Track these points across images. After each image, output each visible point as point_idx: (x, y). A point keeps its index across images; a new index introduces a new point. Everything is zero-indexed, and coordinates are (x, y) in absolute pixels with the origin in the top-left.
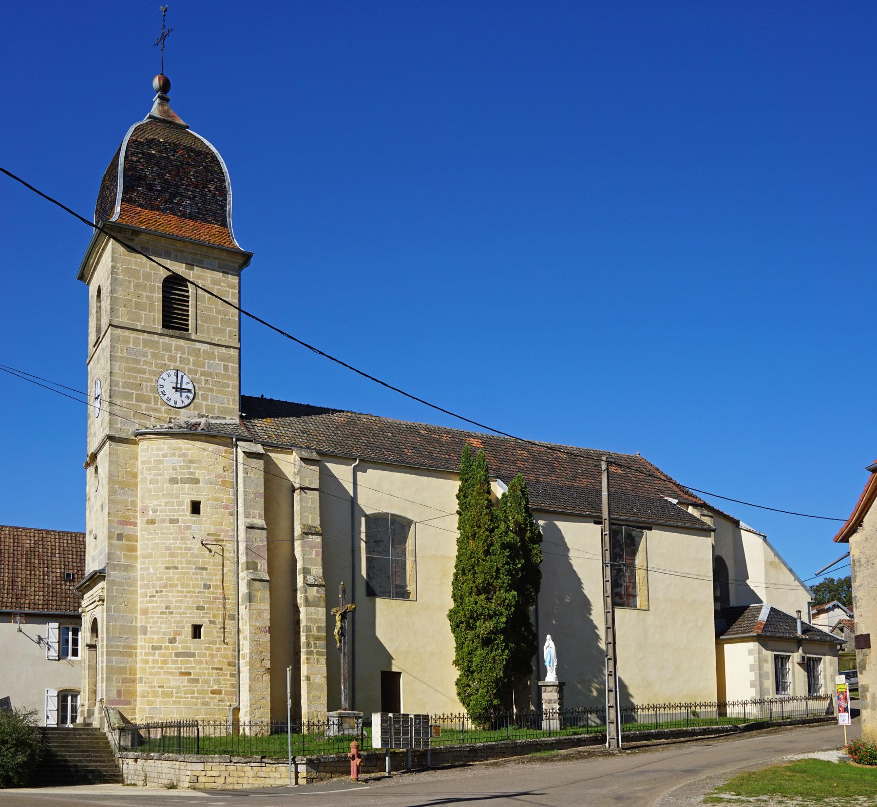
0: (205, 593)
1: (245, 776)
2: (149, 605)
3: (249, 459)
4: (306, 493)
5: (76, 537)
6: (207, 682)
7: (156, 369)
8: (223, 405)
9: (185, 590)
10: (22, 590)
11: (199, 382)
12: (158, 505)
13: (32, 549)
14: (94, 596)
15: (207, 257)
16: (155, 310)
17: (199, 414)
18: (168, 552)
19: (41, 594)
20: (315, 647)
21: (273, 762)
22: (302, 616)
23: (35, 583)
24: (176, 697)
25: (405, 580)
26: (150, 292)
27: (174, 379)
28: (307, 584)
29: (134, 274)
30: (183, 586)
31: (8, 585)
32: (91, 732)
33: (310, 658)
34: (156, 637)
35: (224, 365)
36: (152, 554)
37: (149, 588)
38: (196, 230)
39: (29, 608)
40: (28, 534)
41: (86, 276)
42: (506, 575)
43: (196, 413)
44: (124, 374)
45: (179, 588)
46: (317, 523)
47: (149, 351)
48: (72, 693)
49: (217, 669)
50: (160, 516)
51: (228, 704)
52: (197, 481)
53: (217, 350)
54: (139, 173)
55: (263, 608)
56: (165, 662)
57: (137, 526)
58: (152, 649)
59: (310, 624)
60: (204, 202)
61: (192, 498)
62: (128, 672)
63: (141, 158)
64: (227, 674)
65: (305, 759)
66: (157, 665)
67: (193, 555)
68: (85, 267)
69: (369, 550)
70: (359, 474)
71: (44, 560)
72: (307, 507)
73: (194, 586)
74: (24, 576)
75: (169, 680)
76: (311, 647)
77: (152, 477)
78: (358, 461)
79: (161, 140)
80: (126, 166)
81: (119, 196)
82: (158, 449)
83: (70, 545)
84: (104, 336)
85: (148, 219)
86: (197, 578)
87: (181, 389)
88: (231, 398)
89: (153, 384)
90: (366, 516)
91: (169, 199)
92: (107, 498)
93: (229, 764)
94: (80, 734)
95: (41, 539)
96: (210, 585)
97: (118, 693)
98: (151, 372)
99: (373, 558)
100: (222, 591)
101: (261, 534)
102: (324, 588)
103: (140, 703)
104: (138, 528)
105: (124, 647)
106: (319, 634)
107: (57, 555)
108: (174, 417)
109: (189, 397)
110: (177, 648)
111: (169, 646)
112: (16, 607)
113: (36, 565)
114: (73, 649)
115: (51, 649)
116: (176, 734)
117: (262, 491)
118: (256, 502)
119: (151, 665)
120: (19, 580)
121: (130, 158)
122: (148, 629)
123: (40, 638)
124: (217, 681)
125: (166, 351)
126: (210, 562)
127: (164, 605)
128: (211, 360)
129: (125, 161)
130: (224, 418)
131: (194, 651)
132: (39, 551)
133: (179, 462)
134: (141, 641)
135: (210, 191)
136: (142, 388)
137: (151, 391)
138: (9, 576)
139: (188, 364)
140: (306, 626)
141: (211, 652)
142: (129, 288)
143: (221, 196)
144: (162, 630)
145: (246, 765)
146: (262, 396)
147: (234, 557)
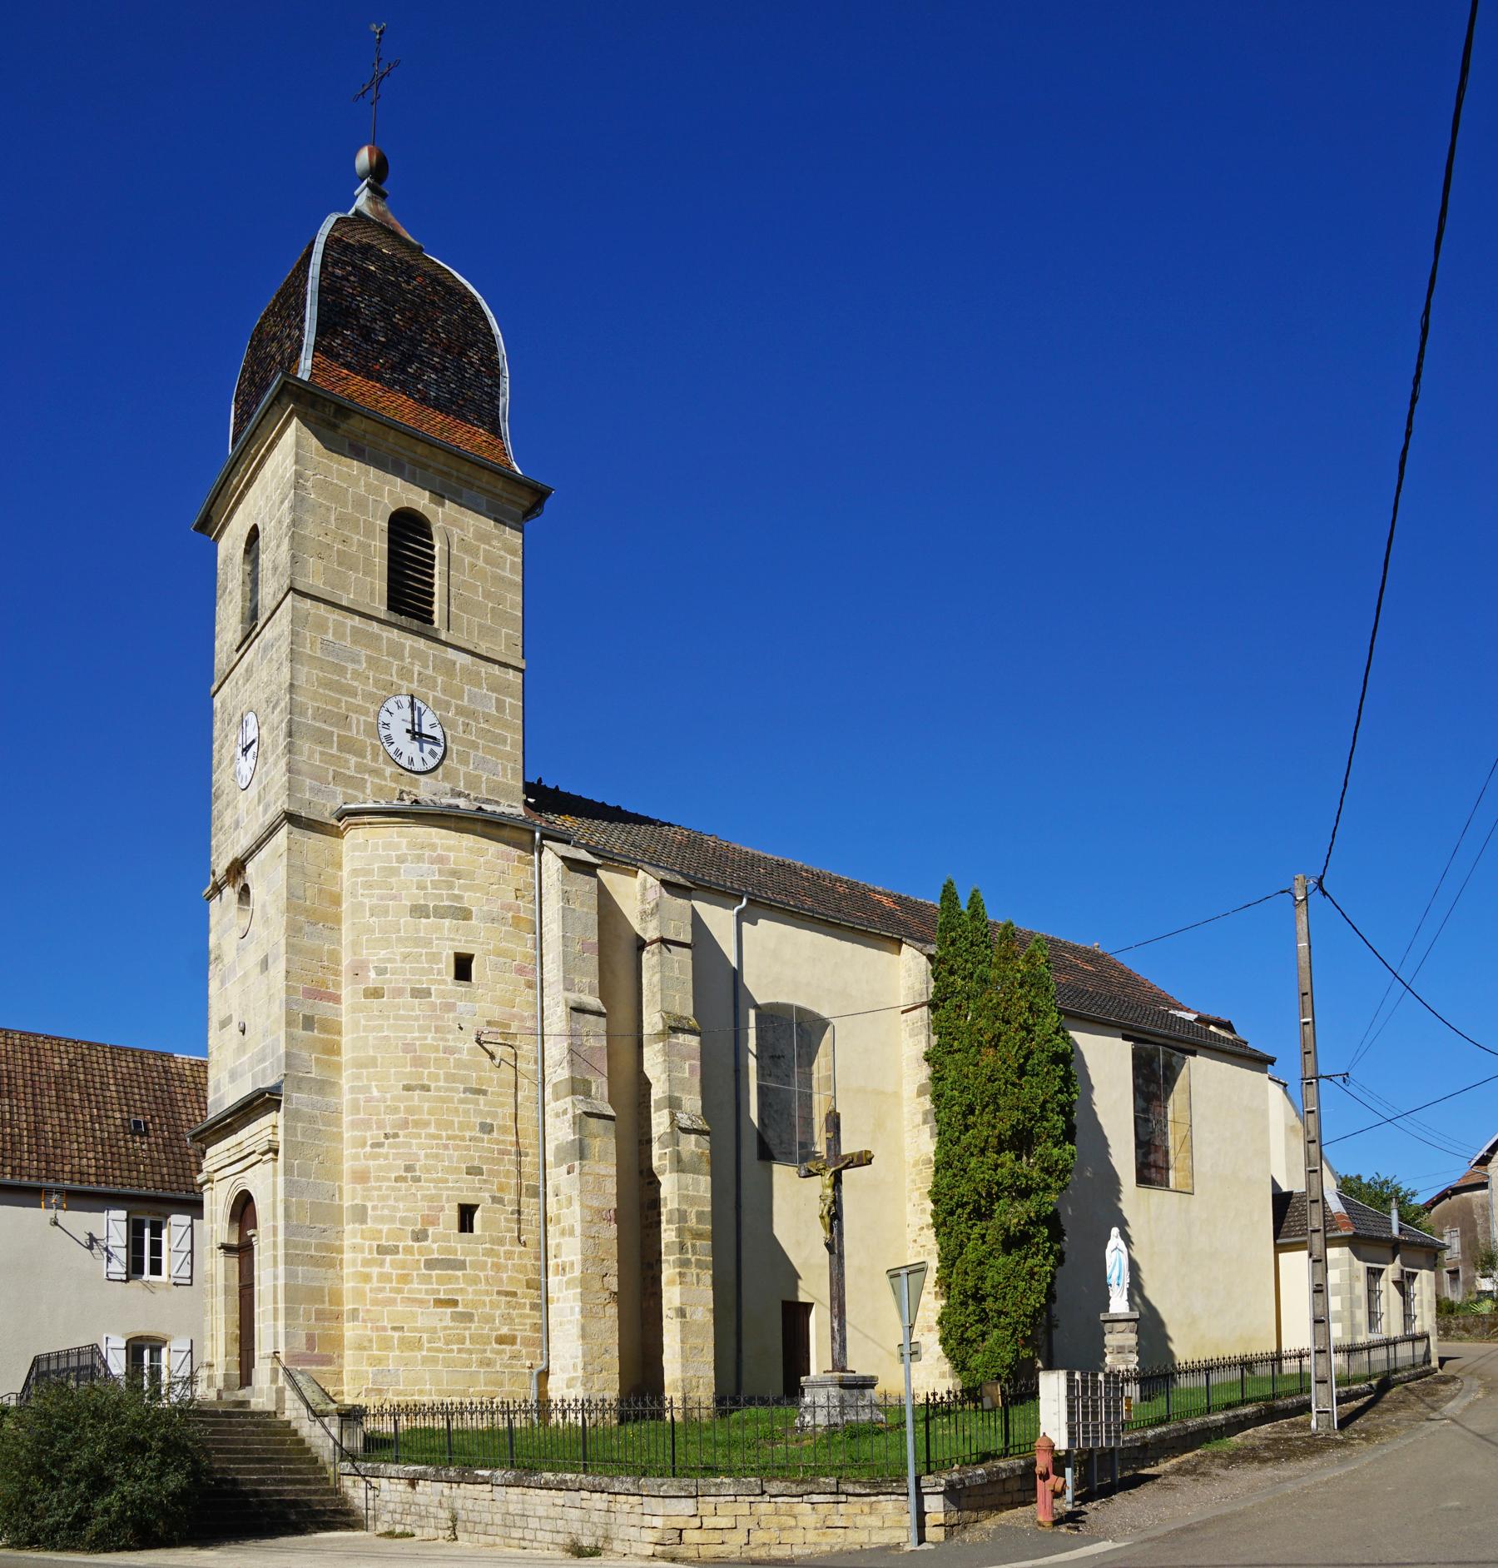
0: (482, 1140)
1: (796, 1527)
2: (371, 1163)
3: (572, 874)
4: (669, 950)
5: (141, 1058)
6: (489, 1319)
7: (375, 690)
8: (495, 778)
9: (444, 1134)
10: (55, 1147)
11: (453, 726)
12: (389, 960)
13: (66, 1074)
14: (245, 1145)
15: (470, 485)
16: (374, 571)
17: (452, 790)
18: (408, 1055)
19: (91, 1155)
20: (694, 1253)
21: (868, 1491)
22: (665, 1192)
23: (78, 1136)
24: (429, 1350)
25: (812, 1133)
26: (364, 536)
27: (406, 713)
28: (680, 1128)
29: (338, 495)
30: (439, 1125)
31: (28, 1137)
32: (260, 1419)
33: (685, 1273)
34: (385, 1228)
35: (497, 699)
36: (375, 1058)
37: (370, 1128)
38: (447, 431)
39: (72, 1180)
40: (56, 1047)
41: (215, 519)
42: (1058, 1114)
43: (448, 786)
44: (315, 692)
45: (432, 1130)
46: (689, 1011)
47: (363, 653)
48: (153, 1344)
49: (507, 1294)
50: (391, 981)
51: (528, 1363)
52: (466, 914)
53: (485, 668)
54: (347, 301)
55: (603, 1172)
56: (404, 1279)
57: (341, 1004)
58: (378, 1253)
59: (684, 1207)
60: (461, 381)
61: (457, 947)
62: (327, 1299)
63: (350, 274)
64: (525, 1304)
65: (943, 1482)
66: (388, 1286)
67: (459, 1064)
68: (216, 498)
69: (761, 1074)
70: (745, 924)
71: (89, 1095)
72: (672, 978)
73: (463, 1126)
74: (56, 1122)
75: (414, 1315)
76: (687, 1252)
77: (375, 901)
78: (745, 901)
79: (384, 251)
80: (324, 283)
81: (309, 338)
82: (388, 846)
83: (133, 1071)
84: (269, 619)
85: (362, 394)
86: (469, 1109)
87: (421, 735)
88: (510, 765)
89: (369, 720)
90: (757, 1007)
91: (399, 363)
92: (283, 942)
93: (759, 1499)
94: (240, 1425)
95: (79, 1057)
96: (492, 1125)
97: (308, 1340)
98: (368, 696)
99: (767, 1087)
100: (514, 1139)
101: (597, 1023)
102: (707, 1138)
103: (350, 1361)
104: (343, 1007)
105: (319, 1247)
106: (700, 1226)
107: (113, 1088)
108: (407, 789)
109: (436, 754)
110: (429, 1250)
111: (412, 1247)
112: (47, 1178)
113: (77, 1103)
114: (152, 1261)
115: (113, 1260)
116: (443, 1424)
117: (595, 939)
118: (584, 960)
119: (375, 1284)
120: (48, 1128)
121: (330, 269)
122: (370, 1212)
123: (92, 1239)
124: (507, 1319)
125: (394, 656)
126: (492, 1079)
127: (401, 1163)
128: (475, 686)
129: (321, 273)
130: (498, 803)
131: (462, 1258)
132: (78, 1079)
133: (431, 873)
134: (351, 1235)
135: (471, 364)
136: (350, 723)
137: (367, 733)
138: (29, 1119)
139: (434, 688)
140: (678, 1210)
141: (495, 1260)
142: (328, 522)
143: (491, 377)
144: (398, 1215)
145: (800, 1499)
146: (540, 781)
147: (536, 1070)
